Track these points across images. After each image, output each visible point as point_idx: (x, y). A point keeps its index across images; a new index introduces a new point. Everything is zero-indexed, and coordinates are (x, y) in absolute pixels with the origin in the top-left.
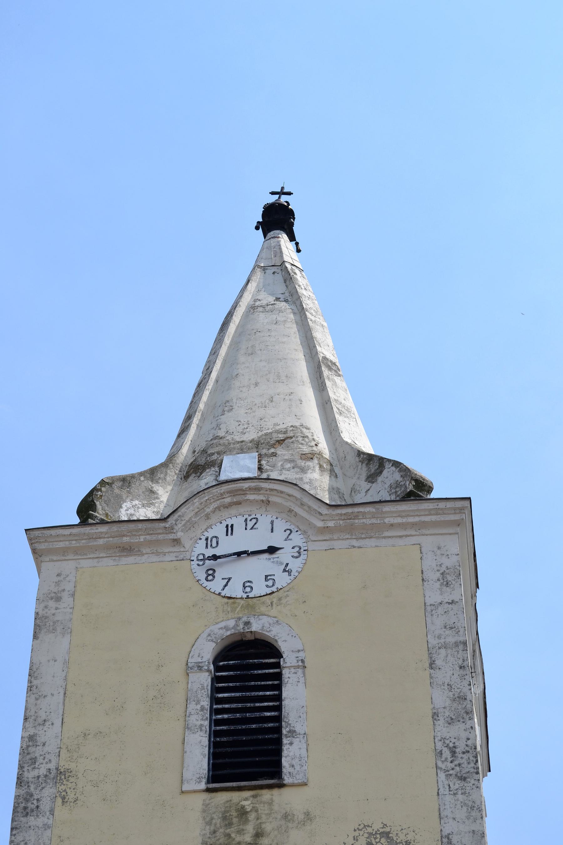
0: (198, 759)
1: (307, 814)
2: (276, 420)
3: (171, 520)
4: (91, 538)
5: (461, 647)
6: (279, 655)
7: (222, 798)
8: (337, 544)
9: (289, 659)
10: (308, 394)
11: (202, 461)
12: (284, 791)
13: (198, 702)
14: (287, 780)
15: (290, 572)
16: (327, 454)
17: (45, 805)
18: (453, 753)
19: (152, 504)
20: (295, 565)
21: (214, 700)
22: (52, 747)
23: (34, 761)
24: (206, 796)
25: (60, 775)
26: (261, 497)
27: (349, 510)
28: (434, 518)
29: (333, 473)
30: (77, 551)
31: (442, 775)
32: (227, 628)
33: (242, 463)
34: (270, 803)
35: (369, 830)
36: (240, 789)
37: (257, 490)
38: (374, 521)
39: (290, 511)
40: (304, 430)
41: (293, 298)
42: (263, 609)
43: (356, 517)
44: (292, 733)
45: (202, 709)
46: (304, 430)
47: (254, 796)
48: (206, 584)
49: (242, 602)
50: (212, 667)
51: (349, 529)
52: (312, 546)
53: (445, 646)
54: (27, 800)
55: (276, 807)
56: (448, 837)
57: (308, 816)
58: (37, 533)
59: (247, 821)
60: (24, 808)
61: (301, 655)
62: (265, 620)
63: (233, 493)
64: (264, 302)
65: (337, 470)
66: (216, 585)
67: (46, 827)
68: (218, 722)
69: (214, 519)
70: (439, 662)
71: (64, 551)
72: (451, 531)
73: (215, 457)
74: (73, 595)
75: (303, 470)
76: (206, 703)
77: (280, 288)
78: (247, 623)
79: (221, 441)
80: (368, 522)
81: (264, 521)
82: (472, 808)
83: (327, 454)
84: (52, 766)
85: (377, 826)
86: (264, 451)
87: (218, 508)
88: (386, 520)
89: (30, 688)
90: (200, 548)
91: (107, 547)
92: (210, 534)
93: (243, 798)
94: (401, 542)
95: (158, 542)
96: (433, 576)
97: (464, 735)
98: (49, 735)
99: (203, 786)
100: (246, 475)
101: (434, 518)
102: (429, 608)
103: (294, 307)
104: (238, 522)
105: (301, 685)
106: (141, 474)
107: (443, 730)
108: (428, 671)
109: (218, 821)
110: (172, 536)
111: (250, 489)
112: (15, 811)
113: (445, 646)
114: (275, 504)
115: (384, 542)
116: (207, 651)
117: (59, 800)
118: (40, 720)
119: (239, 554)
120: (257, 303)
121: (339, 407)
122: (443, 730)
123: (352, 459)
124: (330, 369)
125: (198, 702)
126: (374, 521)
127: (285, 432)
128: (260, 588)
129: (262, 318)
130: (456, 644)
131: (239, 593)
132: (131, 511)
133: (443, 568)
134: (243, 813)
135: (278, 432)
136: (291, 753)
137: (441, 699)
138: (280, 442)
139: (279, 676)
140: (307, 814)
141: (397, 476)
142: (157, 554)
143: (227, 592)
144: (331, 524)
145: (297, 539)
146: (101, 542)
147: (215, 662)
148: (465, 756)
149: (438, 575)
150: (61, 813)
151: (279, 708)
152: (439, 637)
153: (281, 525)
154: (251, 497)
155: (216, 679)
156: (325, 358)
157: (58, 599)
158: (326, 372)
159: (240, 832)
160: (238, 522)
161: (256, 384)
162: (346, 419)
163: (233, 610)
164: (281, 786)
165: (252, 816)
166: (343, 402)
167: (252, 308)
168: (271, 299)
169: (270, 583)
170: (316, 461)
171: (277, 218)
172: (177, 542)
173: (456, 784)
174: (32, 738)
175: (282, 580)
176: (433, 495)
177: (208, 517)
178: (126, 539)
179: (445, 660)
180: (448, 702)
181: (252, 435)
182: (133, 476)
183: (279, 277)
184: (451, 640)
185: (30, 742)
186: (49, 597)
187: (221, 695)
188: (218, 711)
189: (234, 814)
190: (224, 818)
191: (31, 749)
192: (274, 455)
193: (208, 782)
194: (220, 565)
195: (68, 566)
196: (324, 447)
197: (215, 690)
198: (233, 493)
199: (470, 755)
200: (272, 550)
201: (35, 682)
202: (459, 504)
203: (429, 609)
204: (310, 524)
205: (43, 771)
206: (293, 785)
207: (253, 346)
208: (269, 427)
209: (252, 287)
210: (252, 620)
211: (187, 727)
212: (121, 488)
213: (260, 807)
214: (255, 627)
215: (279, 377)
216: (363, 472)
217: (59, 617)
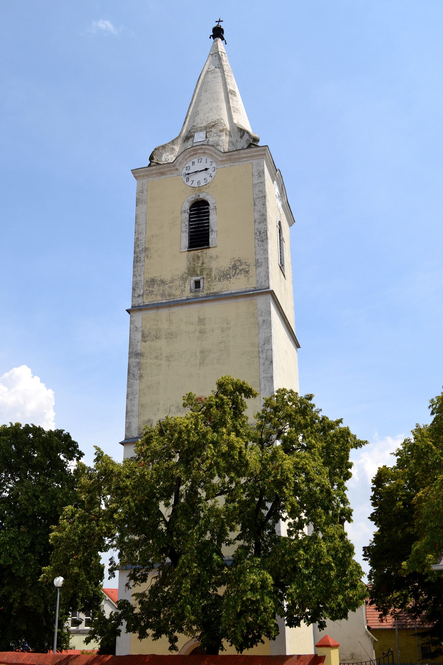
0: (185, 241)
1: (217, 256)
2: (212, 117)
3: (175, 163)
4: (151, 171)
5: (264, 198)
6: (208, 204)
7: (192, 253)
8: (226, 165)
9: (211, 207)
10: (224, 105)
11: (189, 136)
12: (210, 249)
13: (185, 223)
14: (211, 246)
15: (212, 177)
16: (228, 128)
17: (142, 259)
18: (260, 233)
19: (173, 153)
20: (213, 174)
21: (190, 221)
22: (143, 241)
23: (138, 245)
24: (188, 253)
25: (146, 249)
26: (203, 151)
27: (229, 153)
28: (256, 153)
29: (230, 136)
30: (147, 175)
31: (256, 241)
32: (193, 198)
33: (201, 135)
34: (206, 253)
35: (235, 260)
36: (197, 250)
37: (201, 148)
38: (237, 156)
39: (212, 155)
40: (221, 120)
41: (221, 67)
42: (204, 190)
43: (232, 156)
44: (212, 230)
45: (186, 225)
46: (221, 120)
47: (201, 252)
48: (186, 183)
49: (197, 188)
50: (189, 211)
51: (230, 160)
52: (218, 167)
53: (259, 198)
54: (137, 258)
55: (208, 255)
56: (257, 260)
57: (217, 257)
58: (134, 171)
59: (199, 260)
60: (136, 260)
61: (215, 205)
62: (204, 194)
63: (194, 150)
64: (211, 69)
65: (232, 134)
66: (189, 183)
67: (143, 266)
68: (191, 229)
69: (188, 160)
70: (257, 204)
71: (143, 176)
72: (262, 157)
73: (192, 134)
74: (147, 191)
75: (220, 136)
76: (187, 223)
77: (217, 62)
78: (199, 196)
79: (195, 127)
80: (236, 157)
81: (204, 159)
82: (265, 250)
83: (228, 128)
84: (143, 247)
85: (237, 258)
86: (208, 130)
87: (189, 156)
88: (241, 156)
89: (136, 222)
90: (185, 171)
91: (156, 173)
92: (187, 166)
93: (198, 253)
94: (246, 163)
95: (171, 170)
96: (256, 174)
97: (263, 227)
98: (142, 237)
99: (186, 250)
100: (202, 140)
101: (256, 153)
102: (254, 185)
103: (221, 70)
104: (196, 160)
105: (215, 214)
106: (169, 143)
107: (257, 226)
108: (253, 207)
109: (191, 260)
110: (175, 168)
111: (199, 149)
112: (134, 262)
113: (259, 198)
114: (207, 153)
115: (241, 163)
116: (187, 206)
117: (146, 257)
118: (139, 233)
119: (196, 172)
120: (209, 70)
121: (234, 109)
122: (257, 226)
123: (236, 130)
124: (232, 94)
125: (185, 223)
126: (237, 156)
127: (215, 122)
128: (203, 183)
129: (210, 76)
130: (262, 197)
131: (196, 186)
132: (166, 157)
133: (259, 171)
134: (198, 257)
135: (213, 122)
136: (212, 237)
137: (257, 215)
138: (213, 126)
139: (208, 212)
140: (217, 256)
141: (248, 137)
142: (171, 174)
143: (193, 186)
144: (224, 159)
145: (214, 165)
146: (154, 172)
147: (190, 210)
148: (263, 234)
149: (257, 173)
150: (147, 261)
151: (208, 222)
152: (257, 195)
153: (209, 160)
154: (199, 151)
155: (190, 215)
156: (230, 90)
157: (143, 192)
158: (230, 96)
159: (198, 263)
160: (196, 160)
161: (207, 104)
162: (236, 114)
163: (195, 192)
164: (209, 248)
165: (201, 258)
166: (236, 107)
167: (207, 72)
168: (214, 67)
169: (206, 181)
170: (224, 132)
171: (218, 33)
172: (177, 169)
173: (261, 243)
174: (137, 238)
175: (209, 179)
176: (260, 144)
177: (186, 160)
178: (161, 170)
179: (259, 203)
180: (259, 217)
181: (204, 124)
182: (166, 145)
183: (217, 58)
184: (261, 195)
185: (137, 239)
186: (140, 192)
187: (192, 220)
188: (192, 225)
189: (196, 258)
190: (193, 259)
191: (137, 242)
192: (211, 131)
193: (188, 248)
194: (191, 176)
195: (145, 181)
196: (228, 126)
197: (190, 218)
198: (194, 150)
199: (265, 234)
200: (206, 169)
201: (137, 220)
202: (264, 148)
203: (254, 185)
204: (218, 159)
205: (141, 249)
206: (213, 247)
207: (207, 88)
208: (210, 120)
209: (208, 63)
210: (200, 194)
211: (182, 232)
212: (162, 149)
213: (203, 255)
214: (201, 197)
215: (214, 100)
216: (239, 135)
217: (143, 199)
